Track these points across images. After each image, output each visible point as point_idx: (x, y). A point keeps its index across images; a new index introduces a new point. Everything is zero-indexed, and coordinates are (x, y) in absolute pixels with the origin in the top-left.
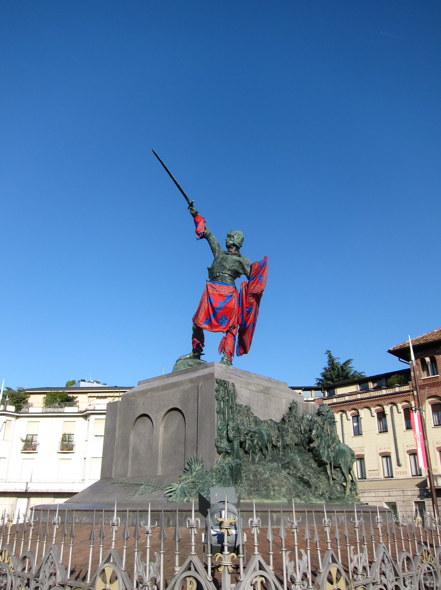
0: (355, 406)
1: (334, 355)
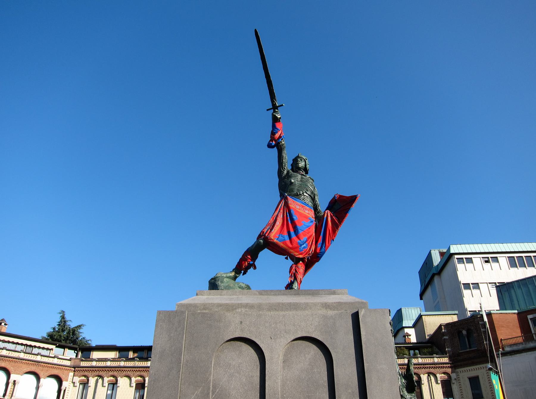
0: (115, 373)
1: (67, 317)
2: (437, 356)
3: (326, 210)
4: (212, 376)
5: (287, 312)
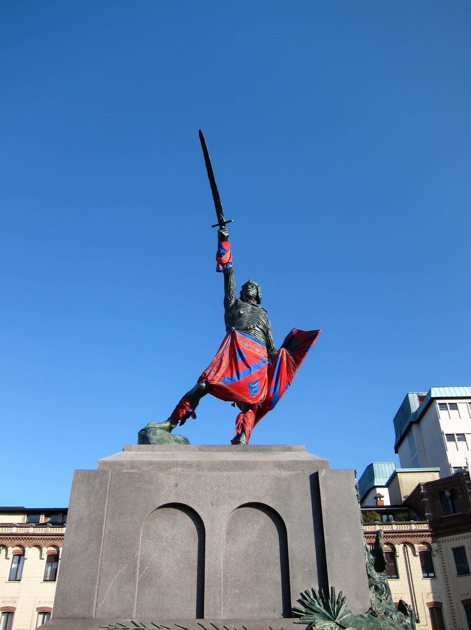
0: (22, 542)
2: (415, 522)
3: (281, 348)
4: (140, 551)
5: (232, 473)
